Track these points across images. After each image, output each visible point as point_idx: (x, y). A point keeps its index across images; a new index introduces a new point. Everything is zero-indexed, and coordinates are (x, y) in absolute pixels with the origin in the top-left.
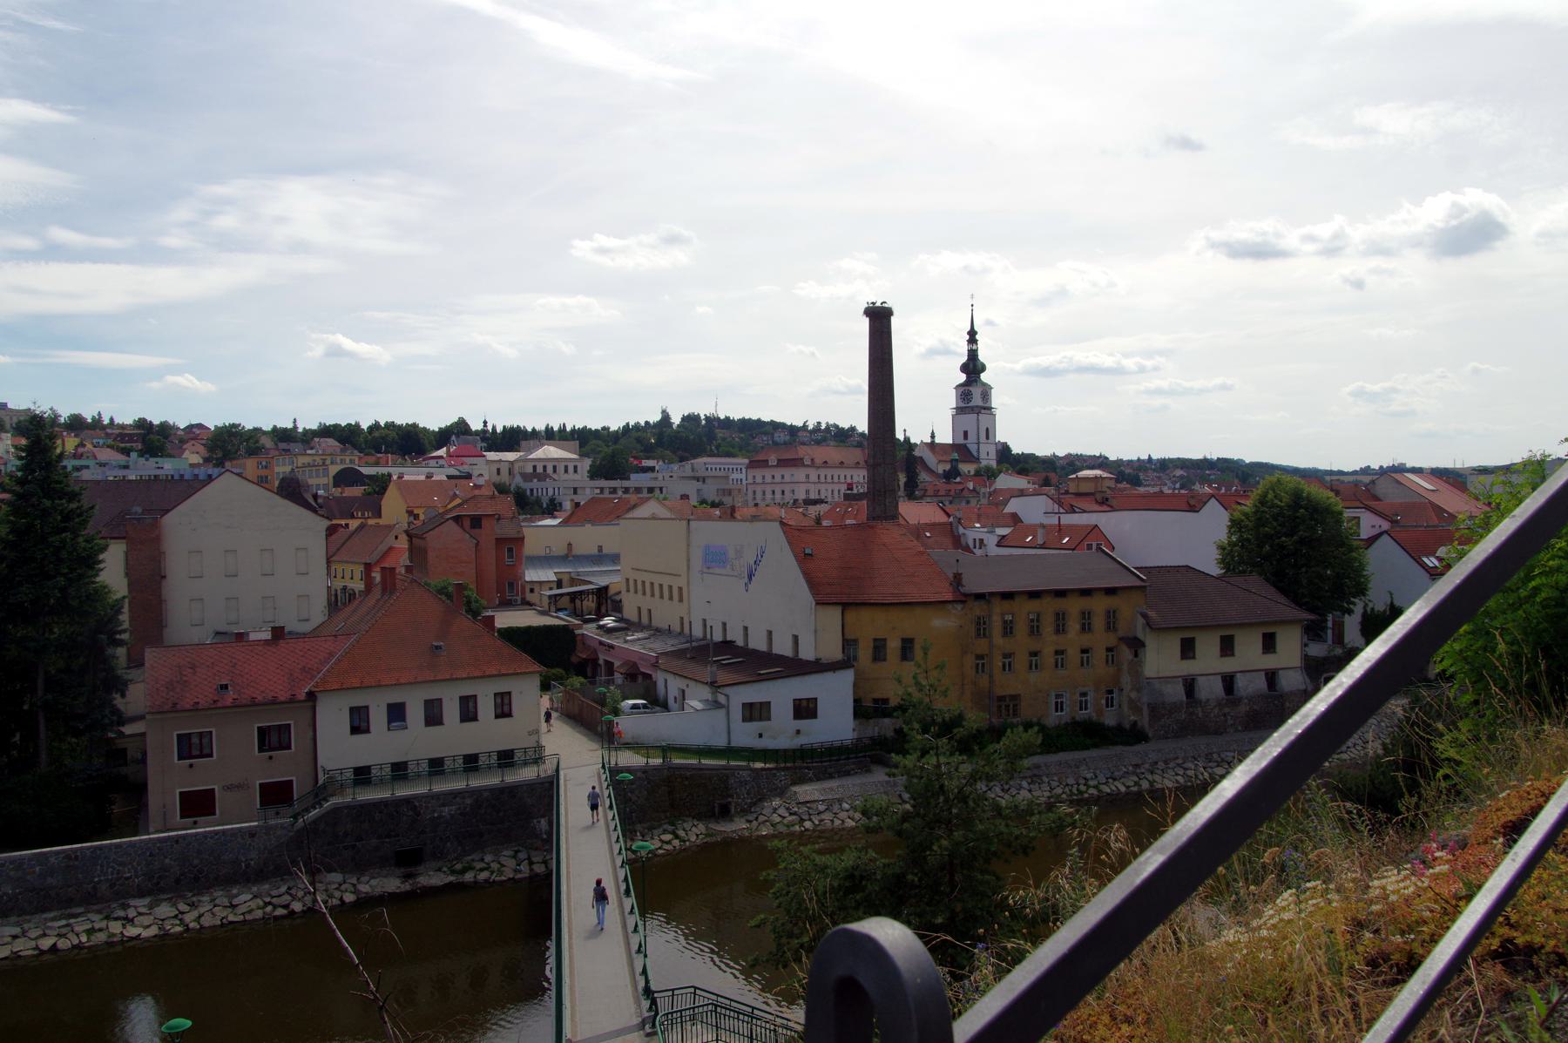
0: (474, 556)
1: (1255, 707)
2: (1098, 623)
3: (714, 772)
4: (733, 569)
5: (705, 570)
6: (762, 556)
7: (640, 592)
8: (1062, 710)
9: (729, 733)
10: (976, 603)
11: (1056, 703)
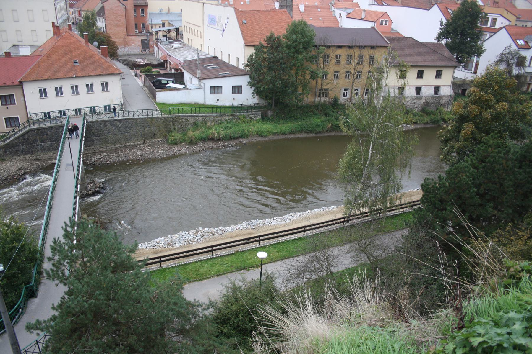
0: (124, 13)
1: (428, 101)
2: (366, 61)
5: (209, 26)
7: (188, 32)
8: (346, 96)
9: (205, 98)
11: (344, 93)
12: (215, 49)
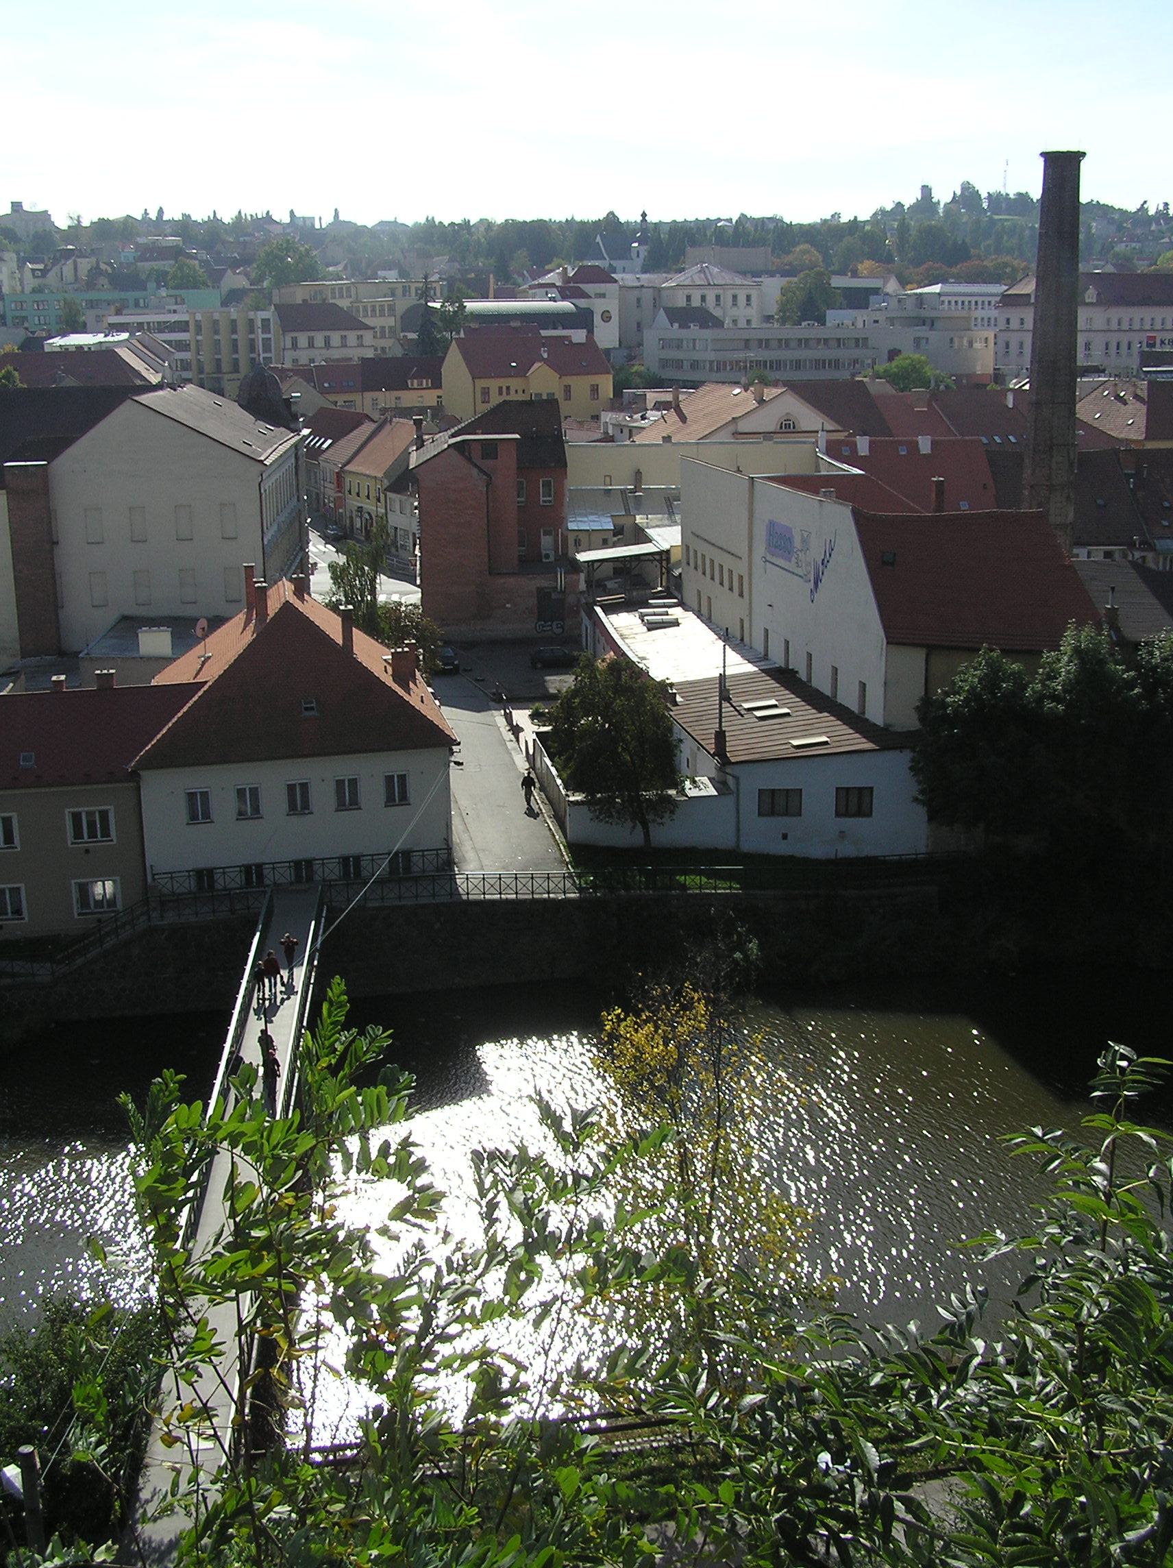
7: (700, 570)
12: (787, 643)
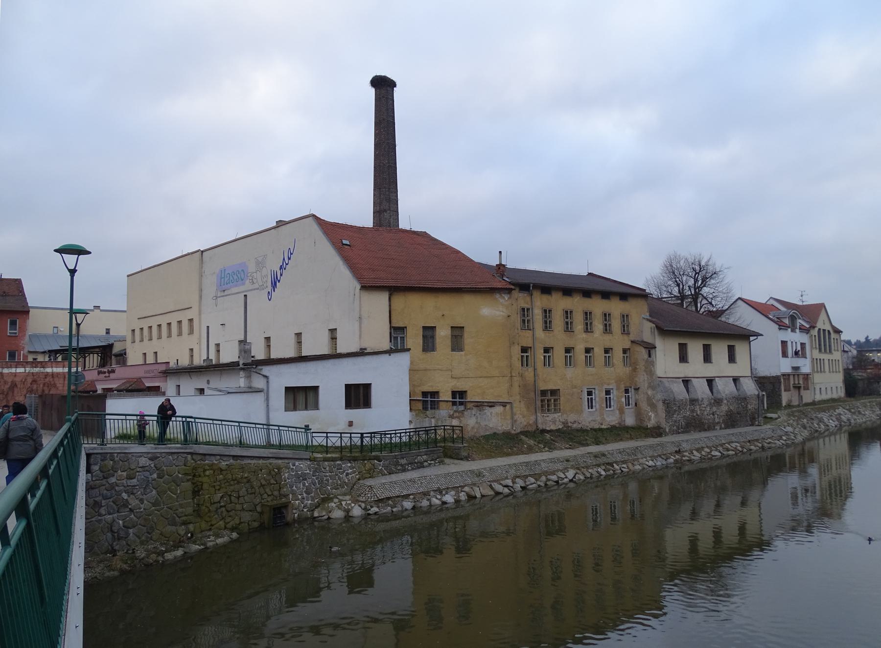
3: (261, 461)
4: (253, 283)
6: (289, 259)
10: (521, 295)
